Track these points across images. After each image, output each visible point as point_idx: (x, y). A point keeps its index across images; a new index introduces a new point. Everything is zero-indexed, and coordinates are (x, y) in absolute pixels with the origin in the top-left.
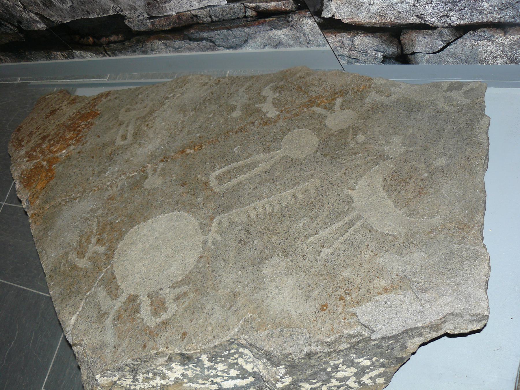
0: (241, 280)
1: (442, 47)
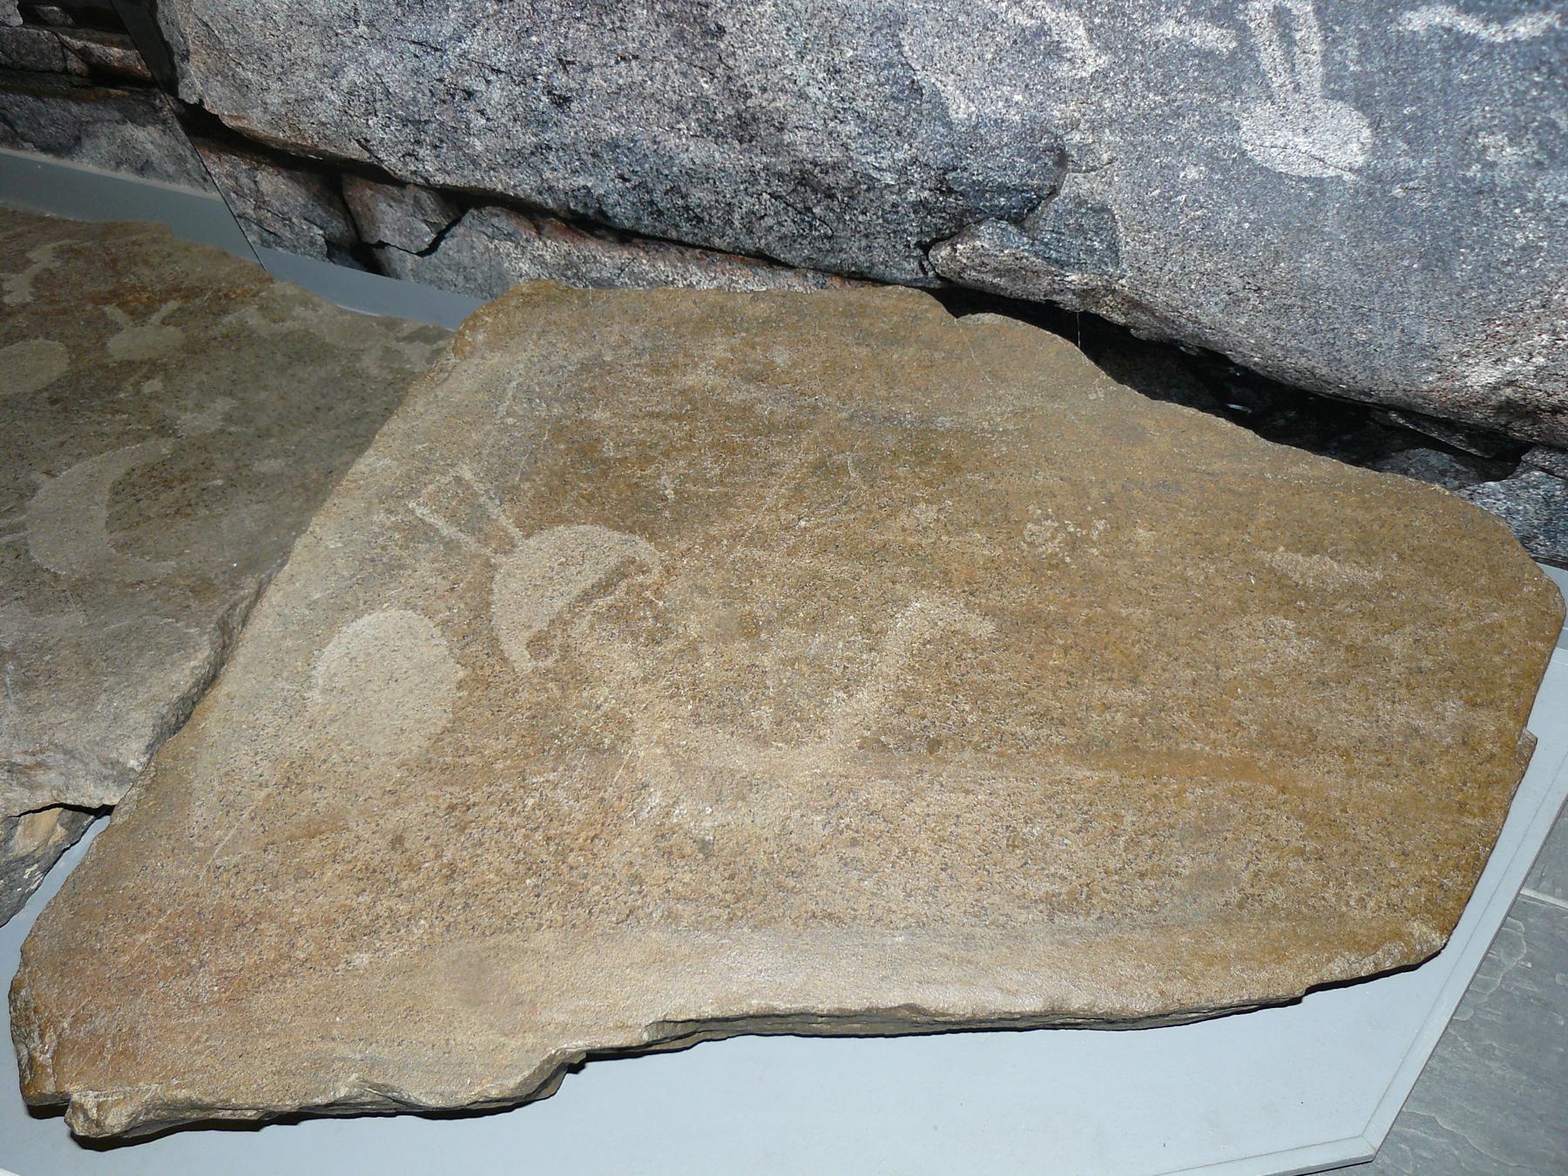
1: (428, 240)
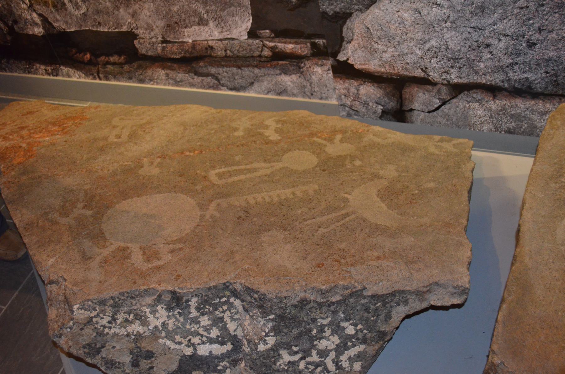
1: (436, 106)
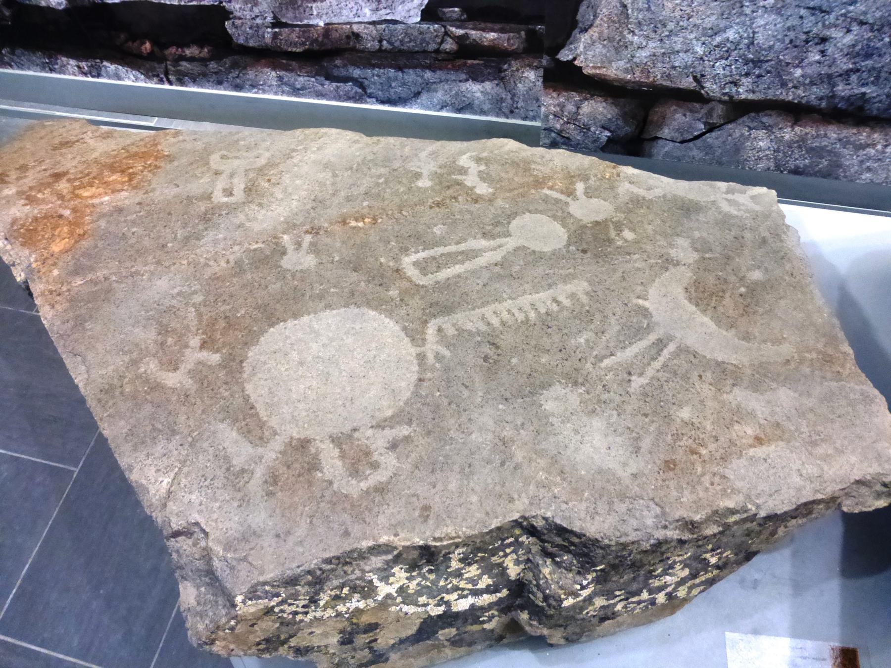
0: (509, 418)
